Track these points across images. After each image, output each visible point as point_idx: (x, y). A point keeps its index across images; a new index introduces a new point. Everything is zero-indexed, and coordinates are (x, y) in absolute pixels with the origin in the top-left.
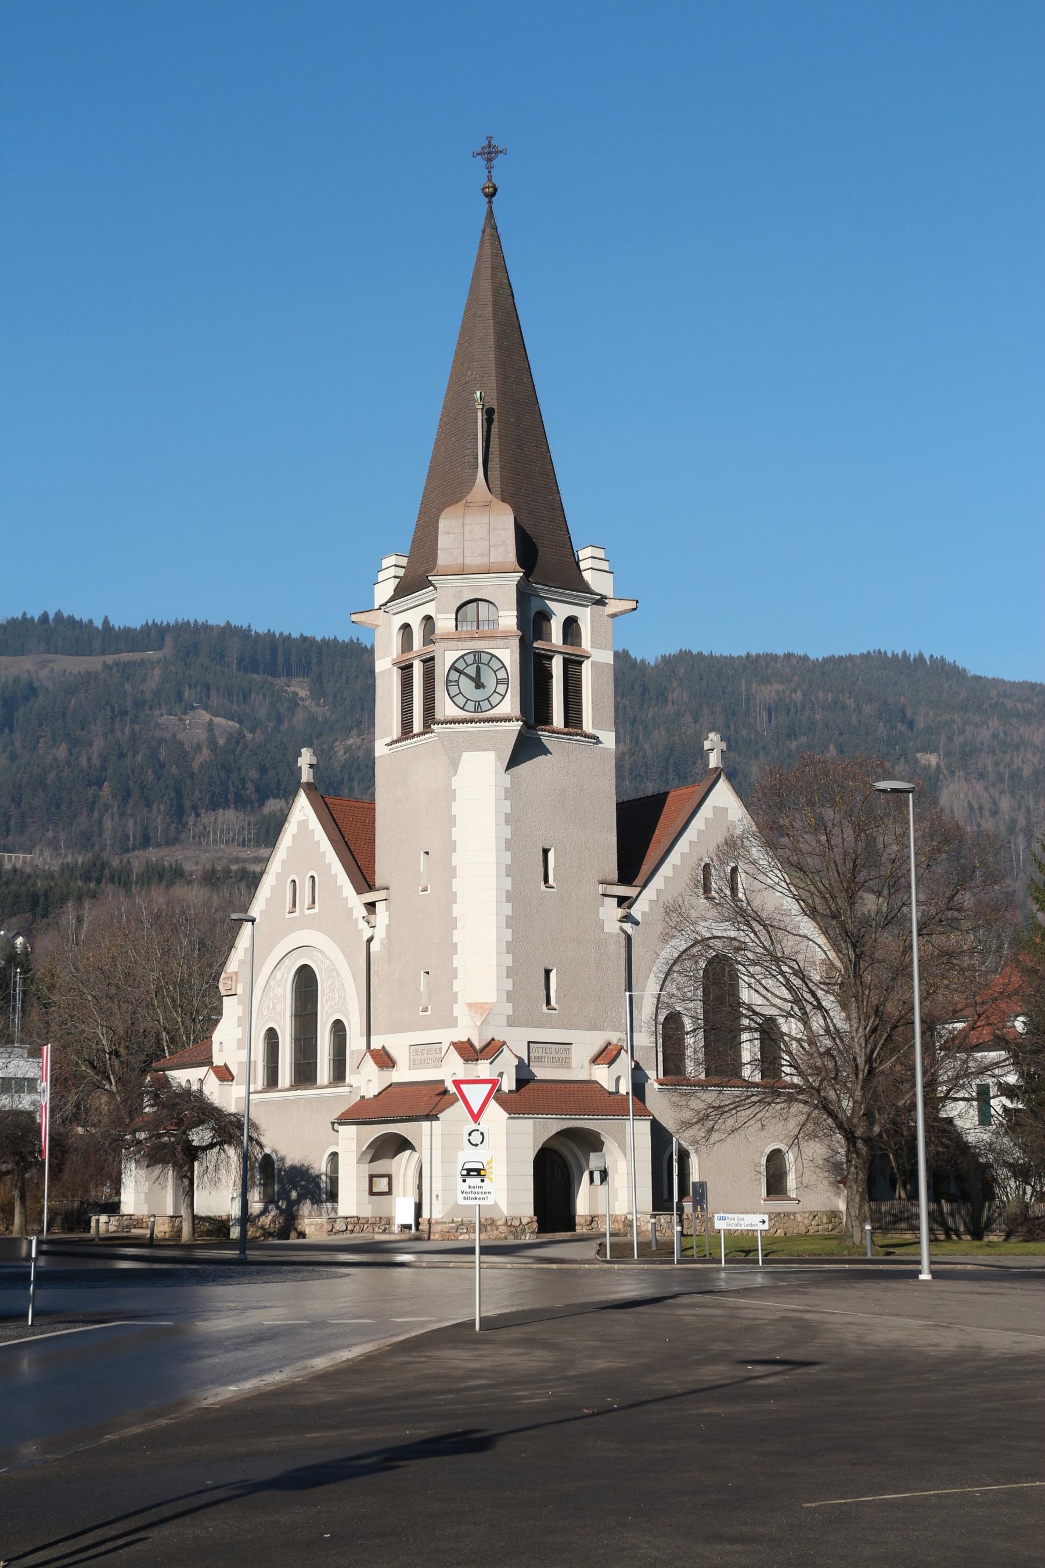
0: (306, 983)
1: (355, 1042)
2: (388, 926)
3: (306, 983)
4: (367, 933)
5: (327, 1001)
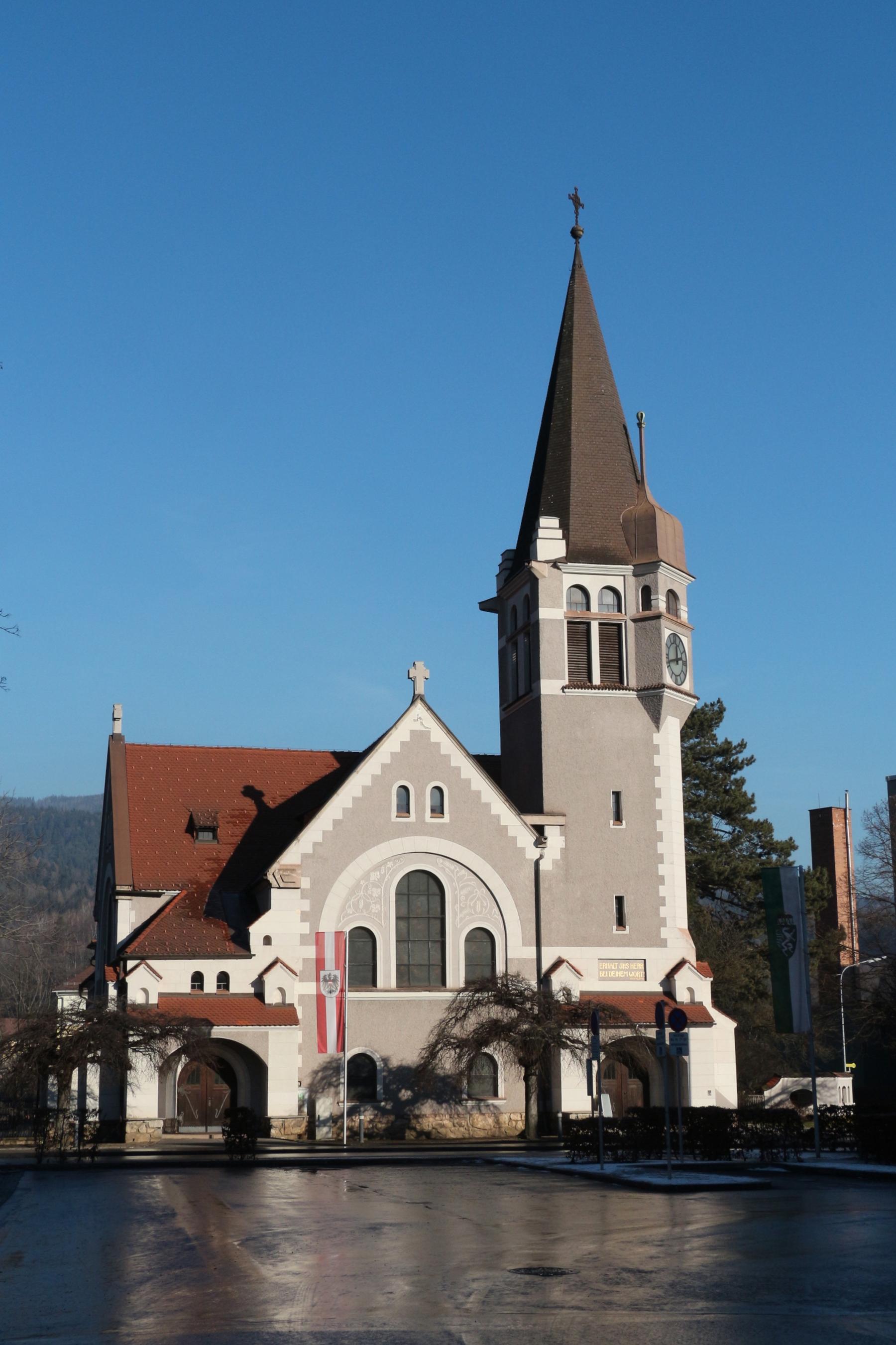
2: (565, 851)
4: (533, 853)
5: (462, 909)
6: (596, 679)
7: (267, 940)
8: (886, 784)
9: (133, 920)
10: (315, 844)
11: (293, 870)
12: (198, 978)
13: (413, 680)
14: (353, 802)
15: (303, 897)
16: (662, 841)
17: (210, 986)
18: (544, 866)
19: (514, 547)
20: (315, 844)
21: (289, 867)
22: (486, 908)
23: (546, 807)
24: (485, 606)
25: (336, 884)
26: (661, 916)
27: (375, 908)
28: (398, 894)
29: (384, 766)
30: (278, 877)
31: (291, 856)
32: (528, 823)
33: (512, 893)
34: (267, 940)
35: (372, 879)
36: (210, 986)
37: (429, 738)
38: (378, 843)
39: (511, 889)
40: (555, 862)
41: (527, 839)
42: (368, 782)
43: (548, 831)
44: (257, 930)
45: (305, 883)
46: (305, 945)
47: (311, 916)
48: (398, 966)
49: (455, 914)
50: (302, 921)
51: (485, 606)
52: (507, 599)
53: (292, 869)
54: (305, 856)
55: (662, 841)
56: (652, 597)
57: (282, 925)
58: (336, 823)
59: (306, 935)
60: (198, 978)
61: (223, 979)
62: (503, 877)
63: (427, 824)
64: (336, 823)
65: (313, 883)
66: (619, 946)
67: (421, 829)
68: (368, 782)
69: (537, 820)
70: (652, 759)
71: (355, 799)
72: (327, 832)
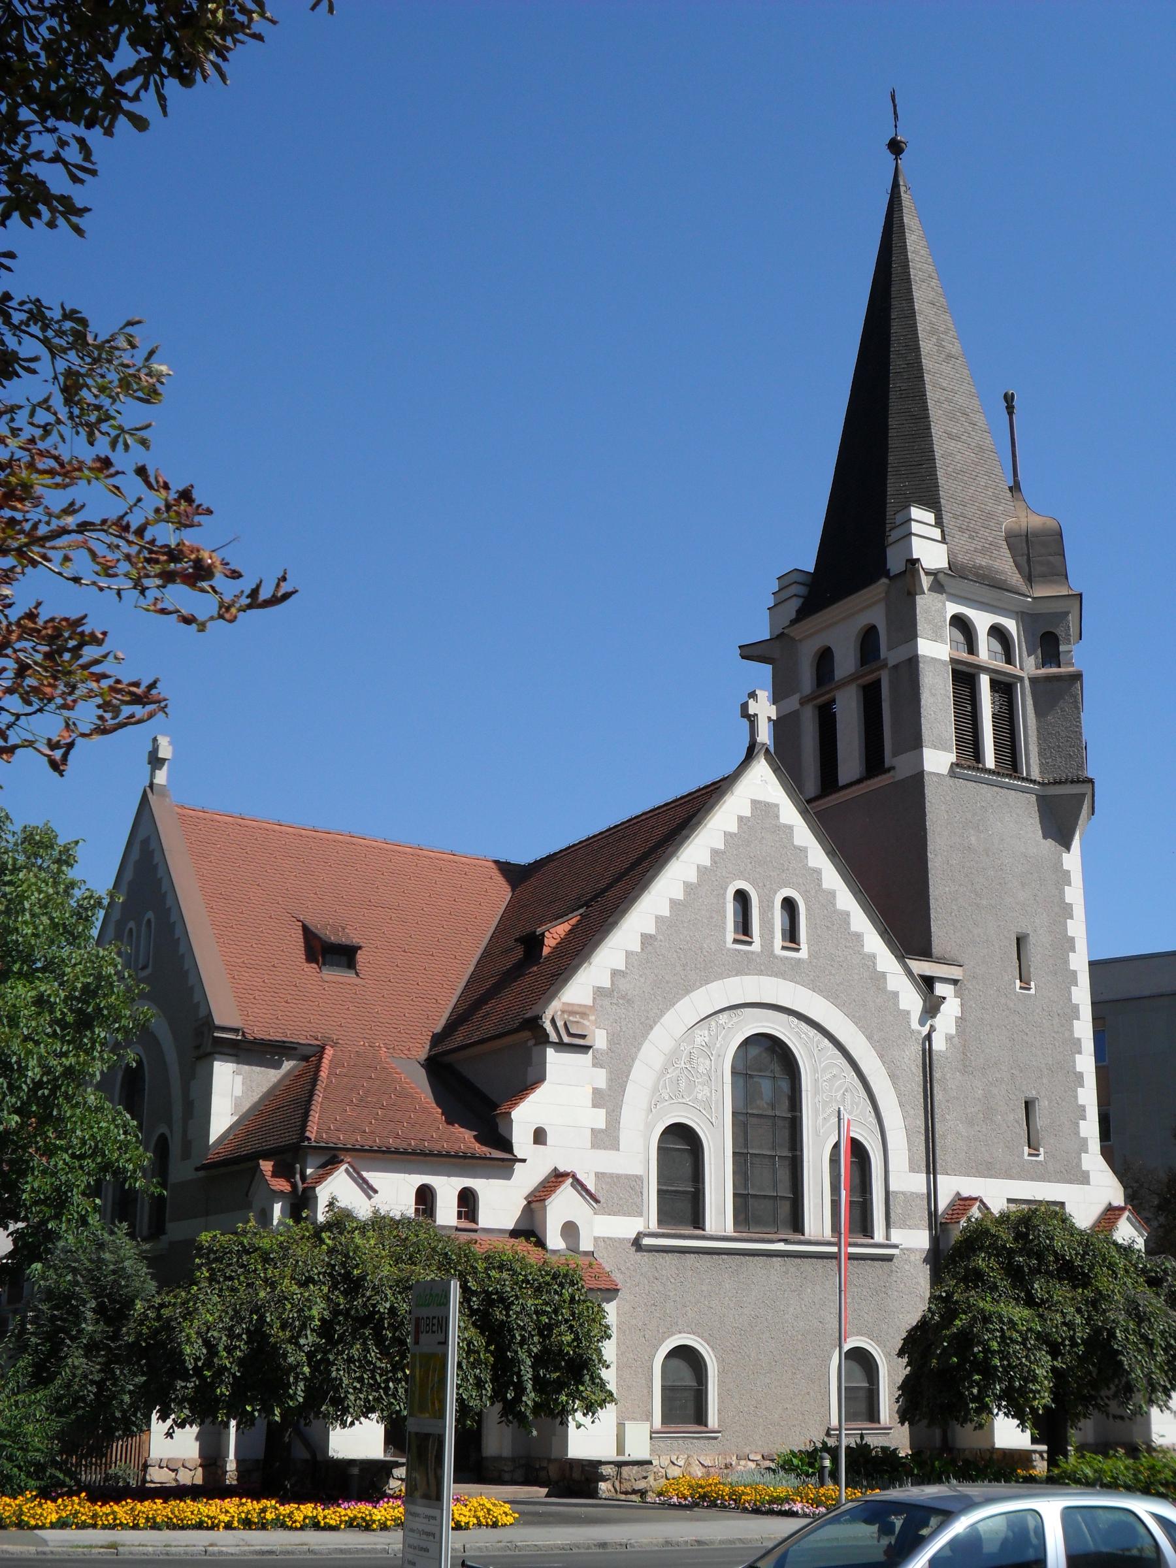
0: (768, 1069)
1: (900, 1174)
2: (961, 1021)
3: (768, 1069)
6: (990, 761)
7: (540, 1136)
8: (422, 1072)
9: (238, 1092)
10: (615, 973)
11: (584, 1015)
12: (425, 1196)
13: (752, 719)
14: (671, 907)
15: (596, 1064)
16: (1078, 1019)
17: (447, 1213)
18: (939, 1044)
19: (810, 567)
20: (615, 973)
21: (576, 1009)
22: (857, 1105)
23: (937, 948)
24: (750, 652)
25: (646, 1046)
26: (1082, 1135)
27: (702, 1092)
28: (734, 1073)
29: (715, 853)
30: (560, 1024)
31: (579, 990)
32: (916, 971)
33: (894, 1083)
34: (540, 1136)
35: (698, 1040)
36: (447, 1213)
37: (778, 817)
38: (707, 982)
39: (893, 1077)
40: (949, 1038)
41: (911, 1001)
42: (693, 877)
43: (940, 989)
44: (524, 1117)
45: (600, 1039)
46: (599, 1148)
47: (609, 1099)
48: (736, 1195)
49: (816, 1112)
50: (594, 1106)
51: (750, 652)
52: (800, 641)
53: (582, 1012)
54: (599, 992)
55: (1078, 1019)
56: (1062, 648)
57: (557, 1110)
58: (646, 939)
59: (601, 1131)
60: (425, 1196)
61: (468, 1201)
62: (881, 1057)
63: (776, 957)
64: (646, 939)
65: (611, 1042)
66: (1032, 1179)
67: (767, 966)
68: (693, 877)
69: (921, 967)
70: (1062, 892)
71: (674, 903)
72: (632, 953)
